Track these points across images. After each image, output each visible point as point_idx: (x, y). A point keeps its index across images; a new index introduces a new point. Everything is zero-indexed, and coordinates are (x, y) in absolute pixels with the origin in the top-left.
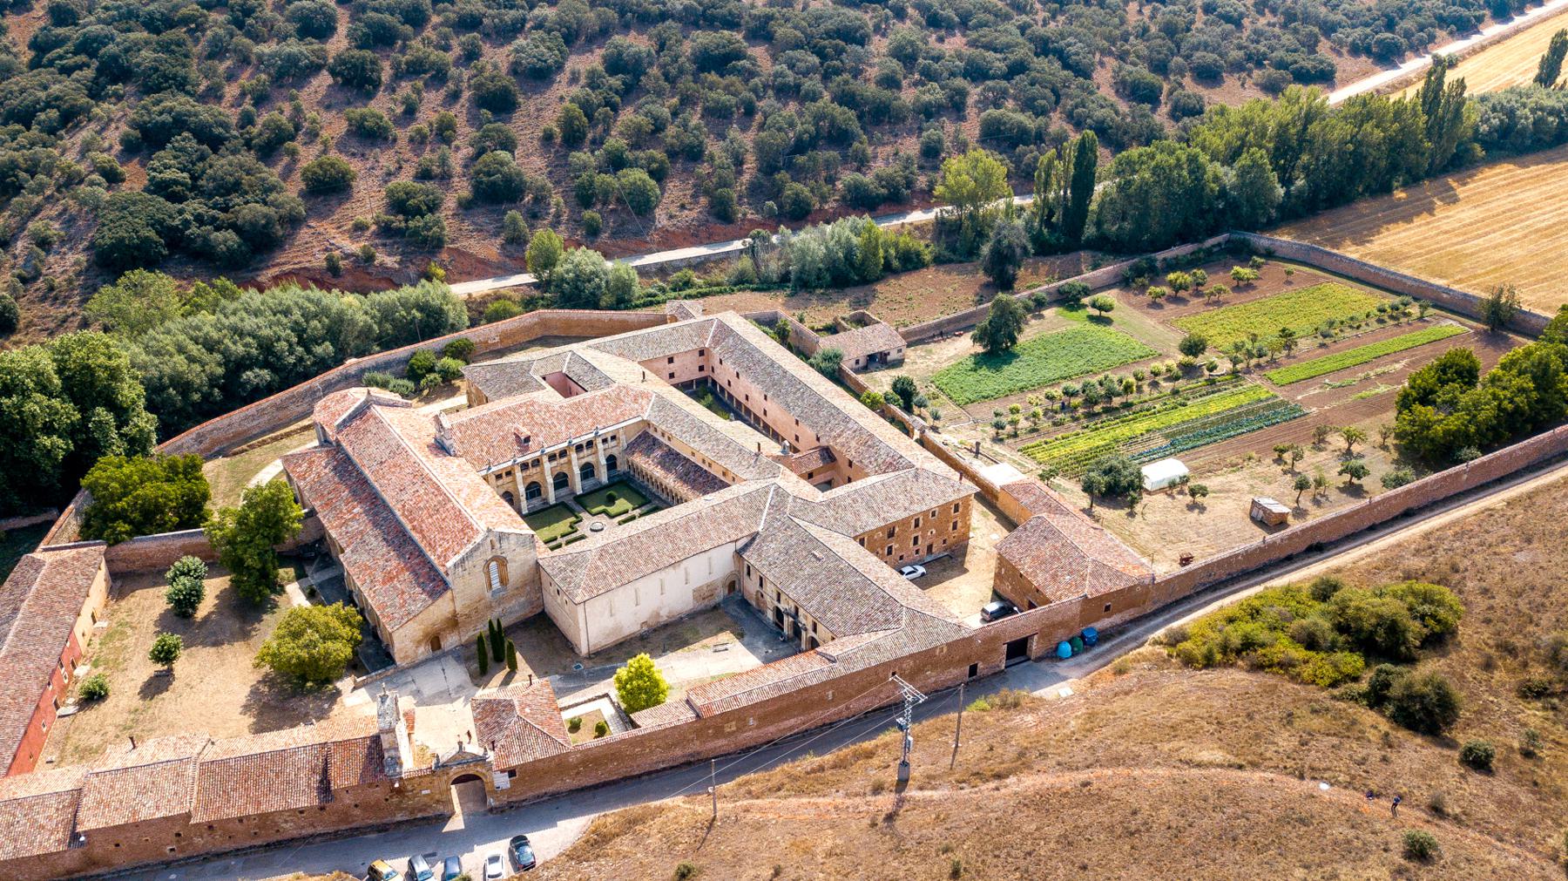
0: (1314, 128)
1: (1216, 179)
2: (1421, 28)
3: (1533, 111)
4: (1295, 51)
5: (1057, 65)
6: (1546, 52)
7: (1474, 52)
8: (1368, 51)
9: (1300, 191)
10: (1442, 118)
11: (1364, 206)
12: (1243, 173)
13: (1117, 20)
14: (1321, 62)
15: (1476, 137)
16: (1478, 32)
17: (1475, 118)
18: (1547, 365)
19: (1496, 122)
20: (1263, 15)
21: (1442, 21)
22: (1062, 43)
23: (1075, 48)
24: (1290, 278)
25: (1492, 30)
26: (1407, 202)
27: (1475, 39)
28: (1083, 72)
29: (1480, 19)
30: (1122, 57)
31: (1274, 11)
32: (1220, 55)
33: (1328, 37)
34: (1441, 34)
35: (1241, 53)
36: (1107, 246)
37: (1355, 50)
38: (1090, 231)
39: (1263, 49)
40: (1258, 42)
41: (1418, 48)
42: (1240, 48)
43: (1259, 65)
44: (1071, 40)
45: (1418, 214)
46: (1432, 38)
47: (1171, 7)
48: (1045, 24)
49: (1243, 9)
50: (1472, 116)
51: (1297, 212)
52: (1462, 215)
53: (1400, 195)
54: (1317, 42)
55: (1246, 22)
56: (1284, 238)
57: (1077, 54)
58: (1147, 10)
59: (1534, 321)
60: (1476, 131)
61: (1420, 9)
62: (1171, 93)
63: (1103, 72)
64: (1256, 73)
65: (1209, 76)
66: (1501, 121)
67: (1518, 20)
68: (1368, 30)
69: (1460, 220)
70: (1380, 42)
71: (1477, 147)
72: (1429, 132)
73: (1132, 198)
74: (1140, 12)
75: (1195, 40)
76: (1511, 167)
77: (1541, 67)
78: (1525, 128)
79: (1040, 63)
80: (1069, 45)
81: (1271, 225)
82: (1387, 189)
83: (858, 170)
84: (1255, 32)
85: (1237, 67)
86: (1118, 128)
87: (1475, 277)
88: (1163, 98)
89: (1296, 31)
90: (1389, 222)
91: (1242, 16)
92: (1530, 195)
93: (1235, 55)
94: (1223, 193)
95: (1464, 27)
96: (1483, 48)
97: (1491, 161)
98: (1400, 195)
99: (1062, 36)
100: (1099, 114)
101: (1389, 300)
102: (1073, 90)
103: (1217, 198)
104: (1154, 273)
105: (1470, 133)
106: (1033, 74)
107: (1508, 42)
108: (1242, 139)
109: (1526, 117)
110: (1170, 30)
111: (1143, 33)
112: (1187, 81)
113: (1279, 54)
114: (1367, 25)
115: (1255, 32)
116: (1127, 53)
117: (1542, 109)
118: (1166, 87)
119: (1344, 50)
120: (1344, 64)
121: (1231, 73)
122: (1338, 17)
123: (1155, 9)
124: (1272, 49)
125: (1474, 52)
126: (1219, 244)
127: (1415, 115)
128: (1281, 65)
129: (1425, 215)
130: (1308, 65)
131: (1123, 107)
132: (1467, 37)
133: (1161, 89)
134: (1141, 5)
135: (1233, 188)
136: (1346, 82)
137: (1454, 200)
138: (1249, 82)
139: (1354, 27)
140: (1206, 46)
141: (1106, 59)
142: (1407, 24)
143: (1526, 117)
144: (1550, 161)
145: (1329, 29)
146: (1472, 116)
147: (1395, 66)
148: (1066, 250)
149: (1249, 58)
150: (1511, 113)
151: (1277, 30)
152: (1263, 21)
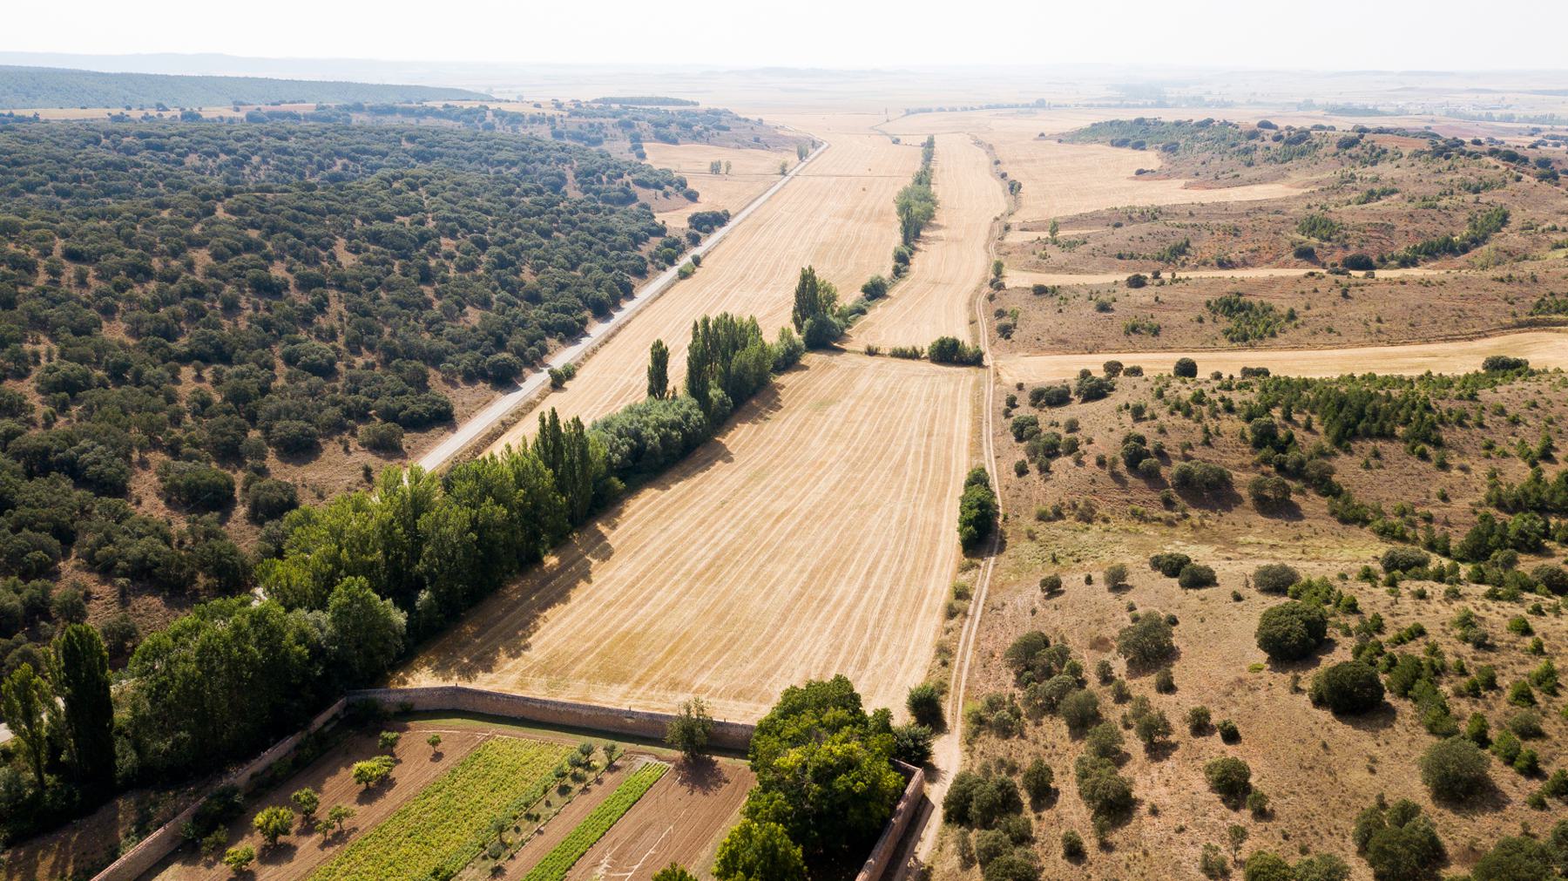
0: (424, 522)
1: (302, 637)
2: (531, 342)
3: (656, 429)
4: (403, 393)
5: (66, 484)
6: (650, 363)
7: (587, 357)
8: (484, 376)
9: (428, 607)
10: (572, 461)
11: (513, 591)
12: (341, 614)
13: (161, 399)
14: (434, 402)
15: (612, 469)
16: (586, 335)
17: (603, 451)
18: (774, 847)
19: (625, 448)
20: (359, 354)
21: (550, 330)
22: (71, 451)
23: (93, 454)
24: (439, 748)
25: (597, 330)
26: (562, 569)
27: (585, 342)
28: (115, 488)
29: (584, 322)
30: (174, 450)
31: (371, 348)
32: (308, 420)
33: (435, 366)
34: (552, 342)
35: (337, 410)
36: (155, 778)
37: (470, 378)
38: (126, 759)
39: (364, 399)
40: (356, 392)
41: (535, 362)
42: (335, 403)
43: (363, 417)
44: (85, 443)
45: (574, 585)
46: (544, 351)
47: (237, 368)
48: (49, 422)
49: (332, 354)
50: (600, 448)
51: (427, 637)
52: (624, 572)
53: (551, 561)
54: (425, 377)
55: (340, 366)
56: (423, 679)
57: (97, 462)
58: (207, 373)
59: (733, 732)
60: (610, 463)
61: (525, 321)
62: (247, 484)
63: (146, 475)
64: (361, 428)
65: (301, 449)
66: (631, 445)
67: (618, 317)
68: (478, 354)
69: (623, 580)
70: (493, 365)
71: (614, 479)
72: (561, 488)
73: (174, 703)
74: (199, 378)
75: (272, 407)
76: (654, 491)
77: (651, 379)
78: (654, 448)
79: (37, 488)
80: (85, 451)
81: (405, 660)
82: (537, 560)
83: (287, 289)
84: (351, 379)
85: (336, 428)
86: (168, 565)
87: (654, 669)
88: (238, 493)
89: (399, 370)
90: (544, 609)
91: (332, 362)
92: (680, 525)
93: (332, 413)
94: (317, 652)
95: (572, 333)
96: (594, 351)
97: (633, 489)
98: (551, 561)
99: (70, 440)
100: (136, 549)
101: (571, 744)
102: (99, 519)
103: (310, 663)
104: (227, 818)
105: (604, 468)
106: (23, 512)
107: (616, 340)
108: (335, 560)
109: (652, 437)
110: (238, 398)
111: (203, 406)
112: (272, 461)
113: (382, 402)
114: (475, 348)
115: (351, 379)
116: (179, 441)
117: (663, 425)
118: (239, 477)
119: (458, 380)
120: (459, 396)
121: (329, 437)
122: (442, 344)
123: (217, 373)
124: (375, 396)
125: (587, 357)
126: (335, 717)
127: (538, 474)
128: (389, 416)
129: (582, 584)
130: (419, 408)
131: (180, 524)
132: (576, 342)
133: (230, 487)
134: (199, 370)
135: (332, 640)
136: (468, 416)
137: (606, 553)
138: (353, 444)
139: (463, 351)
140: (288, 412)
141: (149, 456)
142: (516, 340)
143: (652, 437)
144: (687, 475)
145: (435, 359)
146: (600, 448)
147: (516, 388)
148: (87, 809)
149: (349, 413)
150: (636, 435)
151: (378, 371)
152: (359, 361)
